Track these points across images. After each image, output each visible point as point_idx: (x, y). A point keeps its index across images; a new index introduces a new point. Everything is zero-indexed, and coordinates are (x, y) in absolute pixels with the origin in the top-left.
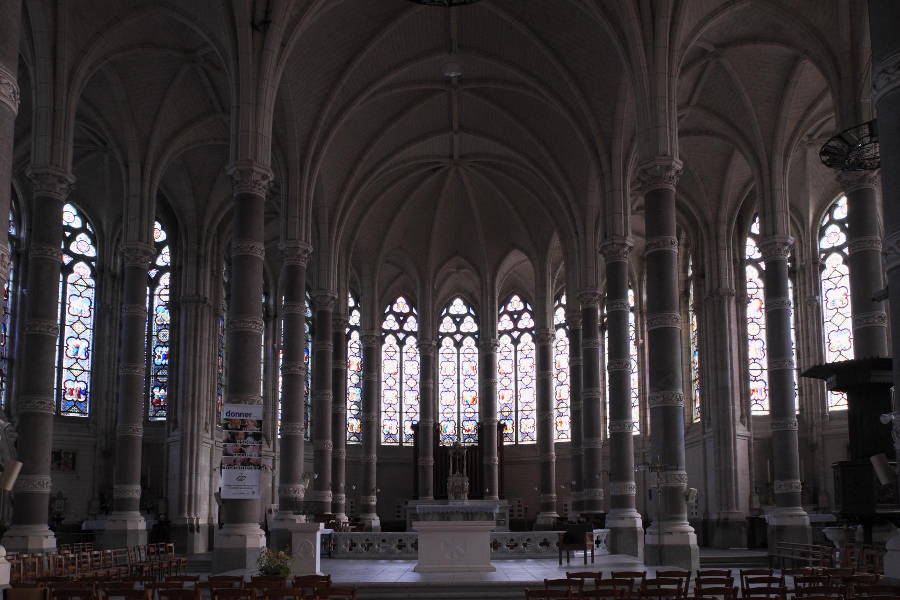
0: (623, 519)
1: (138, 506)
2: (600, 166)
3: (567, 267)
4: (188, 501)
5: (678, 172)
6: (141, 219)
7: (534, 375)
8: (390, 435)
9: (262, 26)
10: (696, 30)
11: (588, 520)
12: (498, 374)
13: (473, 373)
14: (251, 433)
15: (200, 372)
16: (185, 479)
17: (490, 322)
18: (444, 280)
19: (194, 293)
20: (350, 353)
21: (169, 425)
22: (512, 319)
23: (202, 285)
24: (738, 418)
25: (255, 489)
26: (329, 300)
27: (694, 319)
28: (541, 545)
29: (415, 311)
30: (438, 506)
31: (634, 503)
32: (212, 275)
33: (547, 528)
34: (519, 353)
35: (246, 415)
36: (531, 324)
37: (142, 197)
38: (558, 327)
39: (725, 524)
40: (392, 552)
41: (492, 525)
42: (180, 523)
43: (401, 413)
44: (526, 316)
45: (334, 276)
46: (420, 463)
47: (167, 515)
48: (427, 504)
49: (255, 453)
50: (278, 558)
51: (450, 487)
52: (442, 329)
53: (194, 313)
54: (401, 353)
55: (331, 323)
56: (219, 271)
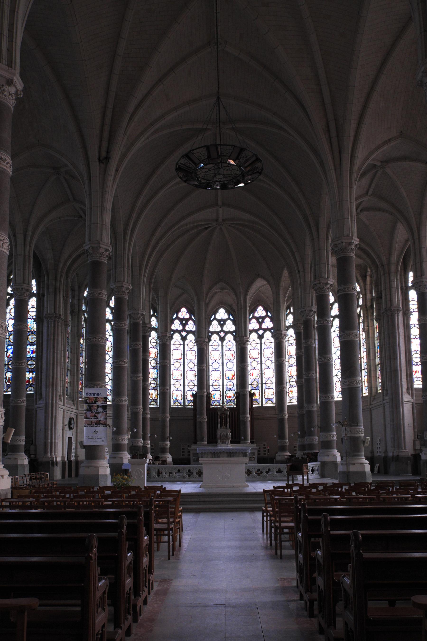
0: (328, 456)
1: (23, 449)
2: (311, 233)
3: (293, 289)
4: (49, 446)
5: (356, 246)
6: (24, 269)
7: (273, 359)
8: (177, 400)
9: (105, 160)
10: (367, 157)
11: (308, 457)
12: (249, 359)
13: (232, 359)
14: (100, 405)
15: (57, 363)
16: (48, 431)
17: (243, 316)
18: (213, 297)
19: (53, 311)
20: (150, 346)
21: (36, 396)
22: (258, 322)
23: (58, 307)
24: (404, 389)
25: (103, 439)
26: (139, 315)
27: (376, 324)
28: (277, 472)
29: (193, 317)
30: (211, 448)
31: (335, 445)
32: (64, 299)
33: (282, 462)
34: (263, 345)
35: (98, 394)
36: (271, 325)
37: (25, 256)
38: (288, 327)
39: (397, 459)
40: (184, 477)
41: (247, 459)
42: (45, 460)
43: (184, 385)
44: (267, 320)
45: (142, 300)
46: (198, 419)
47: (35, 455)
48: (203, 447)
49: (103, 417)
50: (124, 479)
51: (218, 436)
52: (211, 329)
53: (53, 325)
54: (184, 345)
55: (141, 329)
56: (67, 297)
